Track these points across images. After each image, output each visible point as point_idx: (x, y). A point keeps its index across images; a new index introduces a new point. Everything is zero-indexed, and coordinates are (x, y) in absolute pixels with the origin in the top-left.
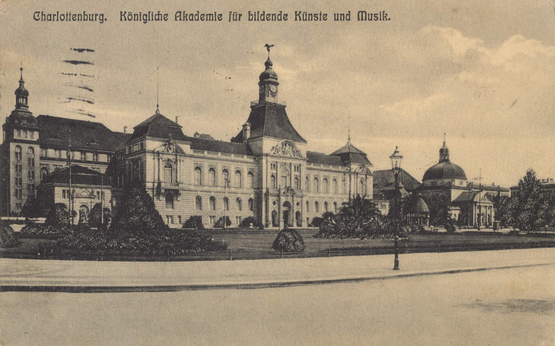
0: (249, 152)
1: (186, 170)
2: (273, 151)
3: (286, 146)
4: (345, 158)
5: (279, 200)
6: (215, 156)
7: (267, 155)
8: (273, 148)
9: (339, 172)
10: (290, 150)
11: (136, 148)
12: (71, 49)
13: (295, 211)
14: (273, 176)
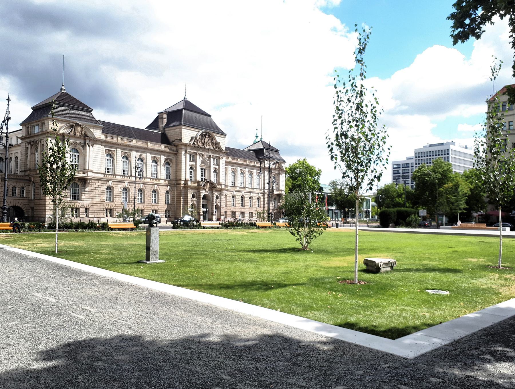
0: (164, 139)
1: (96, 159)
2: (192, 142)
3: (206, 137)
4: (261, 153)
5: (199, 193)
6: (114, 141)
7: (186, 145)
8: (192, 138)
9: (255, 166)
10: (210, 141)
11: (37, 130)
12: (356, 25)
13: (215, 204)
14: (191, 168)
